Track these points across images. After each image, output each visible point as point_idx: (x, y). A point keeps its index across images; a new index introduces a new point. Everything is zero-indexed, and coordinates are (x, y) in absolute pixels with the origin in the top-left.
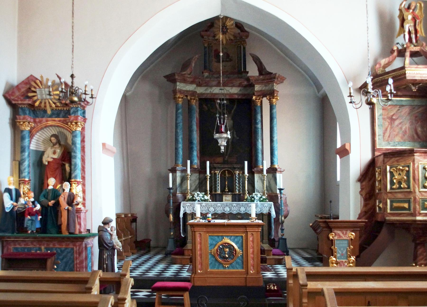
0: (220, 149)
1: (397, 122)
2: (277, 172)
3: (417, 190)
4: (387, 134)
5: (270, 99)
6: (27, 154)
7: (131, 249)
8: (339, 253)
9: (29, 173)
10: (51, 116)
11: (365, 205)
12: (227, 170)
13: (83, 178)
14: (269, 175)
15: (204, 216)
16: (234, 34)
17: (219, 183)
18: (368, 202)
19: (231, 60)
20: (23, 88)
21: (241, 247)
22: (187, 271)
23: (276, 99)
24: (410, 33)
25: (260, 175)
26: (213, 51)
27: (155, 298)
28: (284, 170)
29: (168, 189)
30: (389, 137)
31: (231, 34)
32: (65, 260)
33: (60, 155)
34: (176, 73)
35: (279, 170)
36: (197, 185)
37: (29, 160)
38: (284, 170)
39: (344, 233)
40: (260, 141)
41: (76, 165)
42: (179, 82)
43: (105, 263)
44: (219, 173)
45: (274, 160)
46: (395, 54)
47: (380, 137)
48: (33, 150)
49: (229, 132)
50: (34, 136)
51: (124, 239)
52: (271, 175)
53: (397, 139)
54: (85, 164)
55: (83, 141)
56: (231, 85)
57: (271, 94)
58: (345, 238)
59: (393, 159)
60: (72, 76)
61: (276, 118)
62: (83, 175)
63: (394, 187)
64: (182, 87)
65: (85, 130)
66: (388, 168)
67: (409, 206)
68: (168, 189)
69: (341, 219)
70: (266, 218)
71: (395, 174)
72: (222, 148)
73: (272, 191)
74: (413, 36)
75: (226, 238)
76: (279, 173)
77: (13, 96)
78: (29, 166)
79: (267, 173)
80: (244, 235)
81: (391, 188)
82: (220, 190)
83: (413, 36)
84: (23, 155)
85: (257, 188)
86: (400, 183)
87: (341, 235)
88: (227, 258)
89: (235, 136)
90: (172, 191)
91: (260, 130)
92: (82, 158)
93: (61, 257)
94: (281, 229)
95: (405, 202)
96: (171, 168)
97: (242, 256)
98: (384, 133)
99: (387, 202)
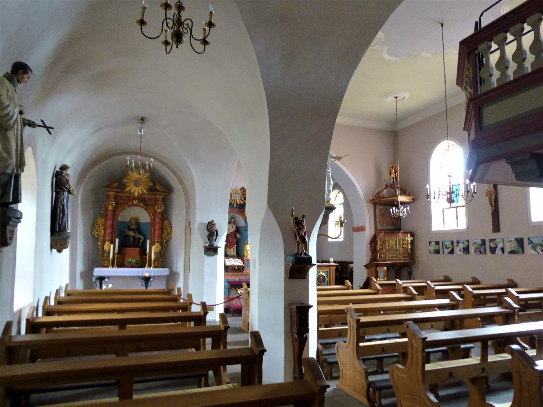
1: (385, 217)
3: (400, 249)
4: (381, 223)
11: (372, 255)
24: (393, 178)
27: (347, 329)
31: (147, 182)
43: (62, 203)
46: (389, 187)
47: (378, 224)
49: (137, 201)
53: (385, 224)
59: (390, 235)
63: (390, 248)
66: (387, 239)
71: (390, 241)
74: (395, 180)
80: (328, 270)
81: (388, 248)
83: (395, 180)
88: (321, 282)
95: (394, 254)
97: (328, 281)
98: (380, 221)
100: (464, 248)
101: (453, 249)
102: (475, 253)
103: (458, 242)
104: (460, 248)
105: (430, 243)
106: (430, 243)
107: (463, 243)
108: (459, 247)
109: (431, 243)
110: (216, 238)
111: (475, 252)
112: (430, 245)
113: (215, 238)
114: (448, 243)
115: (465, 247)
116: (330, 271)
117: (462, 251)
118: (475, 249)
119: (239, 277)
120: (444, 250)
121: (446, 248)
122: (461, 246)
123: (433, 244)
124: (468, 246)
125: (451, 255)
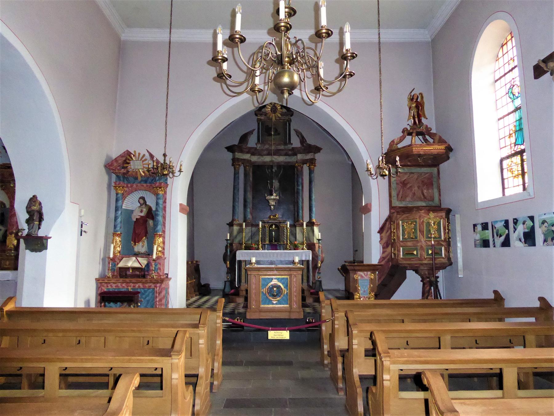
1: (408, 186)
5: (309, 165)
6: (120, 212)
7: (195, 291)
8: (362, 290)
9: (121, 227)
10: (140, 182)
13: (164, 232)
15: (258, 262)
18: (385, 250)
19: (279, 134)
20: (120, 160)
21: (286, 287)
22: (243, 308)
23: (314, 165)
25: (301, 228)
30: (402, 197)
32: (147, 298)
33: (146, 213)
34: (375, 330)
35: (316, 223)
37: (121, 217)
39: (366, 274)
40: (301, 199)
41: (158, 221)
42: (237, 152)
47: (395, 198)
48: (125, 209)
50: (126, 198)
52: (309, 228)
54: (165, 221)
55: (165, 202)
57: (312, 162)
58: (366, 278)
60: (165, 155)
67: (417, 253)
69: (365, 263)
70: (305, 263)
73: (310, 241)
77: (112, 166)
78: (121, 222)
79: (307, 226)
84: (117, 213)
86: (409, 233)
87: (363, 275)
90: (229, 242)
93: (144, 296)
94: (318, 273)
98: (398, 195)
99: (400, 249)
100: (525, 234)
101: (508, 236)
102: (545, 243)
103: (516, 221)
104: (519, 235)
105: (475, 226)
106: (475, 226)
107: (524, 224)
108: (516, 232)
109: (476, 228)
110: (40, 224)
111: (545, 241)
112: (476, 230)
113: (37, 223)
114: (500, 225)
115: (527, 231)
116: (290, 278)
117: (523, 240)
118: (545, 235)
119: (132, 285)
120: (496, 240)
121: (497, 236)
122: (521, 229)
123: (479, 228)
124: (533, 228)
125: (506, 249)
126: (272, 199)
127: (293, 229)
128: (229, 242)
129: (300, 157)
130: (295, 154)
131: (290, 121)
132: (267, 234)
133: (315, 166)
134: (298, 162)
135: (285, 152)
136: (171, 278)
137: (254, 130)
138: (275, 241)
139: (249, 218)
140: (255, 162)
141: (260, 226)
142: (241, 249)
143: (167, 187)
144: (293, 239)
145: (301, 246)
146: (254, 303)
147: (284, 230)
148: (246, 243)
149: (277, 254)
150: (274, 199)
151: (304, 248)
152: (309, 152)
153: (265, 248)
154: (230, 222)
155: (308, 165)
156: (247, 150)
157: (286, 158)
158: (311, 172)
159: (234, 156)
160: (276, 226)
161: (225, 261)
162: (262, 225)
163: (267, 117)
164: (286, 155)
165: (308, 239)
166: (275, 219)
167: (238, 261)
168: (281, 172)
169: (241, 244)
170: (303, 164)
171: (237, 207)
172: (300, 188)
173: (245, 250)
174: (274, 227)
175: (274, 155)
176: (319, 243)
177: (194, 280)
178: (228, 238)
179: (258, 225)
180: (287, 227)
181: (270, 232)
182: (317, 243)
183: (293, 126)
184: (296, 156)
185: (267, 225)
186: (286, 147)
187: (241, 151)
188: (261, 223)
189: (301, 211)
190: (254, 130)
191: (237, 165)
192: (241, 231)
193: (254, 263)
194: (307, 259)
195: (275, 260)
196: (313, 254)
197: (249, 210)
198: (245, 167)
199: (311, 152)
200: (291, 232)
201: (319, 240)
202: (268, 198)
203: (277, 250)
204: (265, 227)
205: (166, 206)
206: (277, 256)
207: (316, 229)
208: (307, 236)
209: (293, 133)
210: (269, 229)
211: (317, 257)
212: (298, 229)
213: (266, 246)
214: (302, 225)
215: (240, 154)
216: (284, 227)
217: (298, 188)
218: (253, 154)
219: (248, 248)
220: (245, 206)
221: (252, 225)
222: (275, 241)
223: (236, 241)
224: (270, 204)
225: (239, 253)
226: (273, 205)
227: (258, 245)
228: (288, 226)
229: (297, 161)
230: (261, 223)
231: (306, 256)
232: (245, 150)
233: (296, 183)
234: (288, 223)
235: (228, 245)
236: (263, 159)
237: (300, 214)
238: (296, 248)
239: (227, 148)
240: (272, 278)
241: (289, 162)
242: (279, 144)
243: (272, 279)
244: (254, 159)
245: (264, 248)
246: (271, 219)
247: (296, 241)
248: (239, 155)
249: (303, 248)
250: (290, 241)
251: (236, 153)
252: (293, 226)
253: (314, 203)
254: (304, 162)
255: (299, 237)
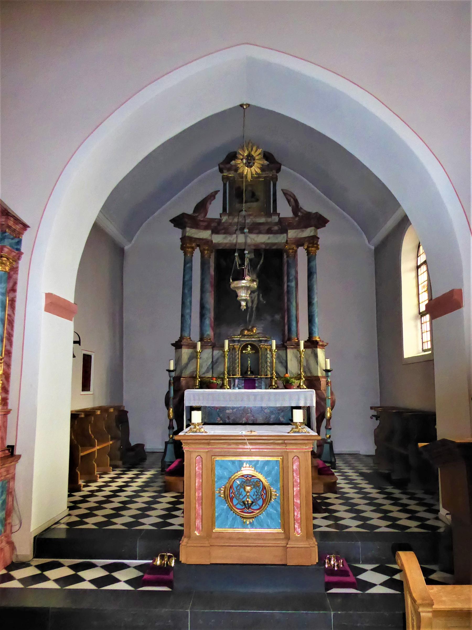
0: (240, 305)
2: (318, 347)
5: (308, 247)
12: (251, 345)
14: (307, 350)
16: (261, 166)
17: (238, 358)
19: (257, 200)
25: (295, 350)
26: (234, 189)
28: (327, 344)
29: (167, 370)
35: (320, 343)
36: (209, 365)
38: (327, 344)
40: (294, 304)
44: (239, 348)
45: (314, 330)
51: (98, 448)
52: (309, 351)
56: (257, 231)
57: (313, 241)
61: (316, 273)
62: (8, 348)
64: (193, 233)
65: (17, 271)
68: (167, 370)
72: (243, 304)
73: (311, 372)
75: (248, 465)
76: (321, 347)
79: (305, 347)
82: (240, 372)
85: (290, 370)
89: (261, 299)
91: (294, 290)
92: (9, 318)
96: (175, 342)
126: (242, 287)
127: (282, 353)
128: (173, 374)
129: (292, 234)
130: (284, 231)
131: (275, 179)
132: (238, 361)
133: (317, 248)
134: (289, 242)
135: (267, 227)
136: (19, 456)
137: (216, 192)
138: (252, 373)
139: (208, 335)
140: (219, 244)
141: (226, 348)
142: (193, 387)
143: (19, 258)
144: (281, 369)
145: (296, 381)
146: (198, 522)
147: (267, 354)
148: (203, 376)
149: (255, 395)
150: (247, 288)
151: (302, 384)
152: (306, 227)
153: (234, 385)
154: (177, 340)
155: (306, 247)
156: (205, 224)
157: (269, 238)
158: (311, 258)
159: (184, 233)
160: (253, 347)
161: (167, 404)
162: (229, 345)
163: (239, 174)
164: (269, 231)
165: (308, 369)
166: (251, 335)
167: (187, 407)
168: (262, 261)
169: (194, 378)
170: (298, 246)
171: (187, 317)
172: (293, 284)
173: (201, 388)
174: (249, 349)
175: (251, 232)
176: (327, 376)
177: (111, 442)
178: (172, 368)
179: (223, 346)
180: (271, 350)
181: (244, 358)
182: (323, 377)
183: (282, 184)
184: (285, 235)
185: (237, 345)
186: (269, 220)
187: (196, 225)
188: (227, 342)
189: (294, 324)
190: (216, 192)
191: (188, 248)
192: (194, 357)
193: (199, 424)
194: (308, 405)
195: (251, 405)
196: (317, 395)
197: (207, 322)
198: (202, 252)
199: (311, 227)
200: (278, 357)
201: (327, 371)
202: (234, 284)
203: (254, 388)
204: (234, 349)
205: (15, 297)
206: (255, 400)
207: (320, 352)
208: (305, 364)
209: (280, 195)
210: (242, 352)
211: (324, 400)
212: (290, 353)
213: (237, 381)
214: (298, 345)
215: (194, 231)
216: (266, 349)
217: (289, 284)
218: (215, 231)
219: (205, 384)
220: (202, 316)
221: (214, 347)
222: (252, 373)
223: (187, 373)
224: (239, 298)
225: (188, 393)
226: (245, 300)
227: (223, 379)
228: (274, 347)
229: (287, 241)
230: (227, 342)
231: (306, 399)
232: (202, 224)
233: (285, 279)
234: (274, 342)
235: (172, 379)
236: (232, 239)
237: (294, 328)
238: (287, 385)
239: (172, 221)
240: (240, 461)
241: (274, 244)
242: (259, 216)
243: (241, 463)
244: (218, 239)
245: (232, 385)
246: (245, 336)
247: (287, 373)
248: (191, 232)
249: (300, 384)
250: (276, 373)
251: (188, 229)
252: (283, 346)
253: (316, 310)
254: (299, 243)
255: (293, 366)
